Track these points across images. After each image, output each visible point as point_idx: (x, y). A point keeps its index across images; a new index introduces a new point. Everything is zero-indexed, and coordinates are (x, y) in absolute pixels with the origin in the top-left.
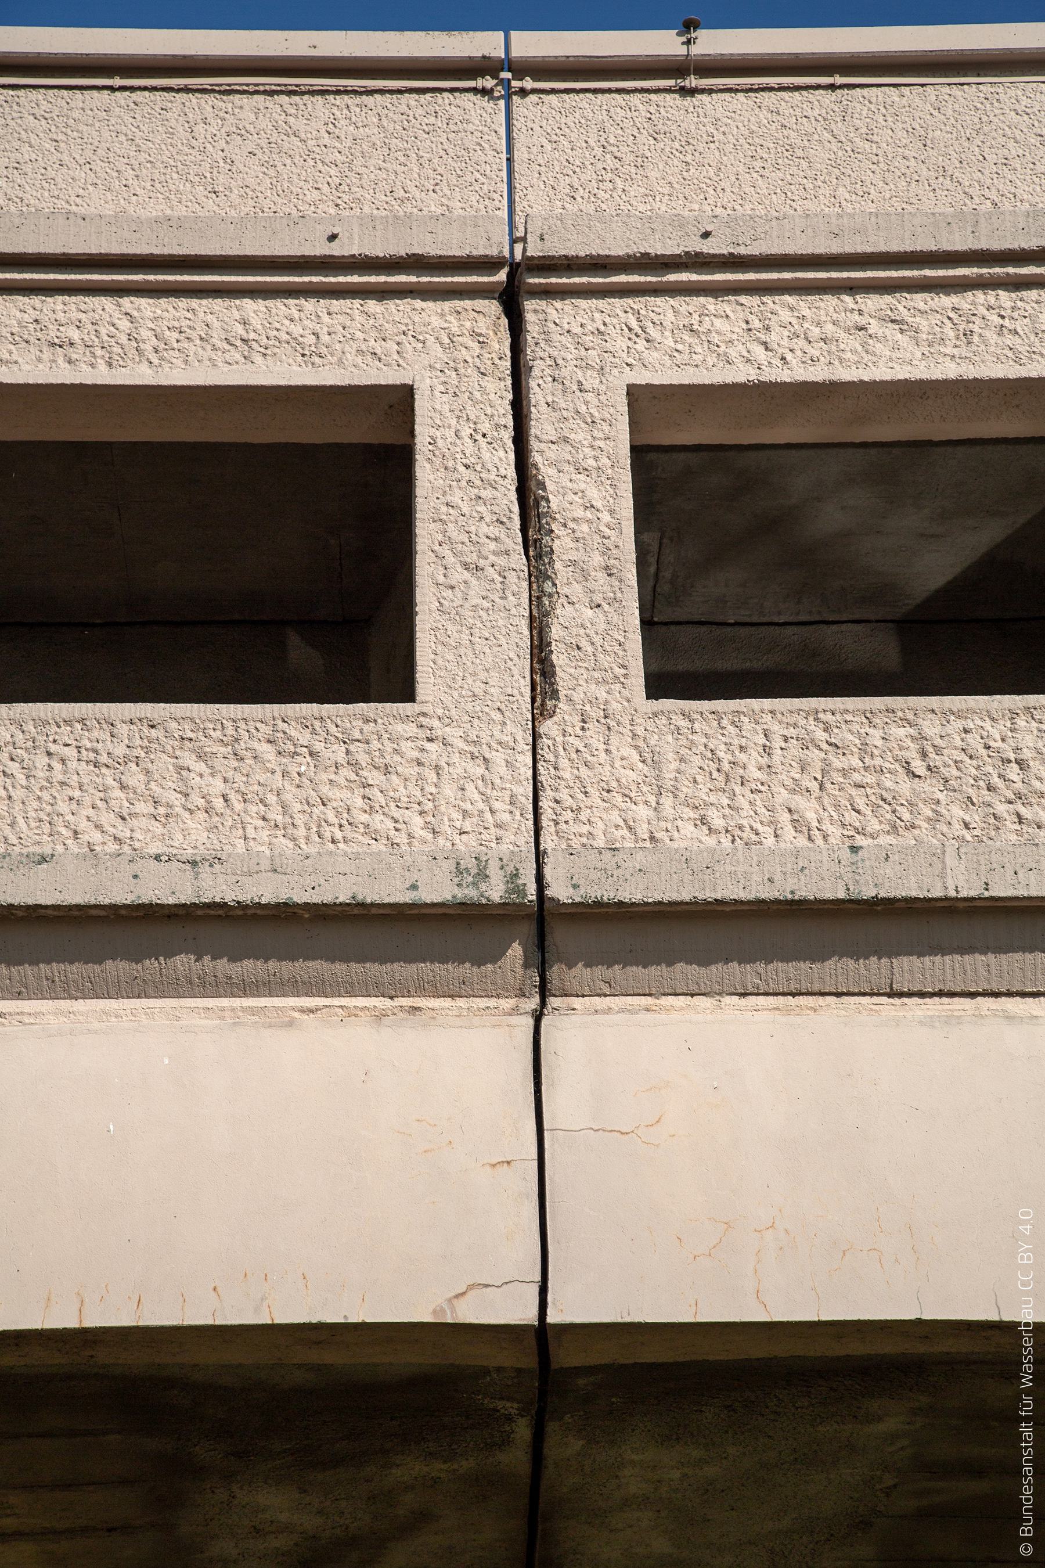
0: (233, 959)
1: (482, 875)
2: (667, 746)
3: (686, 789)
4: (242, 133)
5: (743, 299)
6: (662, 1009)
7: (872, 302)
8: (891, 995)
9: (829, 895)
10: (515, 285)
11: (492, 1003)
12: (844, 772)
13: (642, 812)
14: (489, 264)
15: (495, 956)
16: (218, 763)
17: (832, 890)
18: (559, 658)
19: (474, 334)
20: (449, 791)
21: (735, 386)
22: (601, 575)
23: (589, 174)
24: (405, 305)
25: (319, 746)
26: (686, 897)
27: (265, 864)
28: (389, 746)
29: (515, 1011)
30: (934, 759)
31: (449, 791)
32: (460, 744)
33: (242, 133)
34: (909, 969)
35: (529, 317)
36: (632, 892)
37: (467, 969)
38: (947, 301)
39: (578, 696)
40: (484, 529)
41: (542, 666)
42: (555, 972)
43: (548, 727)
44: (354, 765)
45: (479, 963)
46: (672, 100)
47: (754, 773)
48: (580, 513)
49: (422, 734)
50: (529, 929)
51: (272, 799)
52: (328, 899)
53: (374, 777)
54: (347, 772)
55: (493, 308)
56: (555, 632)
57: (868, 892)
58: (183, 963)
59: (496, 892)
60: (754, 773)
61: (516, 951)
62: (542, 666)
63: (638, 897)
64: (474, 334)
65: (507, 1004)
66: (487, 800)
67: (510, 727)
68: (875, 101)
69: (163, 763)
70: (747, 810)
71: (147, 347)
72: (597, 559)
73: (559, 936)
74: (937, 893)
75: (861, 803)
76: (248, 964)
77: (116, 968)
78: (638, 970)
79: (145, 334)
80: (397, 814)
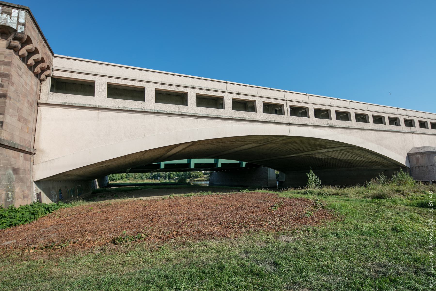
10: (287, 100)
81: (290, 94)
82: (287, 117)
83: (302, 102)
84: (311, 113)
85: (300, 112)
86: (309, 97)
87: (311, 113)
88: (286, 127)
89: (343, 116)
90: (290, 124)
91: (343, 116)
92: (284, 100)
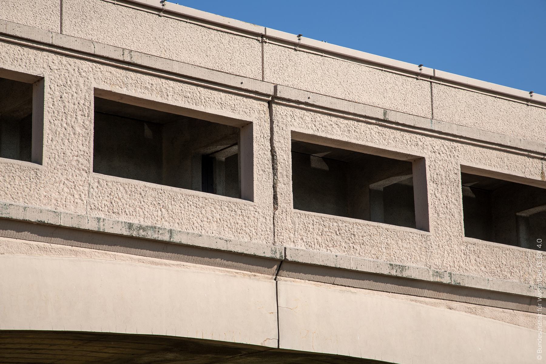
0: (227, 261)
1: (276, 252)
2: (297, 220)
3: (300, 231)
4: (211, 40)
5: (312, 113)
6: (296, 281)
7: (334, 119)
8: (334, 284)
9: (332, 266)
10: (273, 100)
11: (268, 276)
12: (326, 232)
13: (292, 235)
14: (268, 96)
15: (271, 267)
16: (218, 210)
17: (333, 265)
18: (278, 196)
19: (263, 111)
20: (259, 224)
21: (310, 135)
22: (285, 177)
23: (277, 68)
24: (251, 100)
25: (236, 210)
26: (309, 263)
27: (239, 243)
28: (249, 212)
29: (272, 278)
30: (341, 232)
31: (259, 224)
32: (261, 213)
33: (211, 40)
34: (338, 280)
35: (273, 109)
36: (300, 260)
37: (266, 269)
38: (346, 121)
39: (282, 206)
40: (266, 162)
41: (275, 198)
42: (280, 272)
43: (277, 212)
44: (243, 215)
45: (268, 268)
46: (293, 51)
47: (311, 230)
48: (282, 161)
49: (255, 210)
50: (279, 263)
51: (228, 221)
52: (250, 253)
53: (246, 219)
54: (241, 217)
55: (266, 104)
56: (278, 190)
57: (338, 266)
58: (218, 260)
59: (278, 257)
60: (311, 230)
61: (276, 267)
62: (275, 198)
63: (301, 261)
64: (263, 111)
65: (270, 277)
66: (266, 228)
67: (270, 211)
68: (329, 60)
69: (208, 209)
70: (309, 238)
71: (203, 101)
72: (285, 173)
73: (284, 265)
74: (349, 268)
75: (328, 239)
76: (229, 262)
77: (207, 259)
78: (294, 273)
79: (203, 98)
80: (250, 228)
81: (303, 56)
82: (267, 213)
83: (383, 122)
84: (444, 201)
85: (380, 185)
86: (438, 88)
87: (444, 201)
88: (257, 286)
89: (351, 180)
90: (282, 265)
91: (351, 180)
92: (257, 95)
